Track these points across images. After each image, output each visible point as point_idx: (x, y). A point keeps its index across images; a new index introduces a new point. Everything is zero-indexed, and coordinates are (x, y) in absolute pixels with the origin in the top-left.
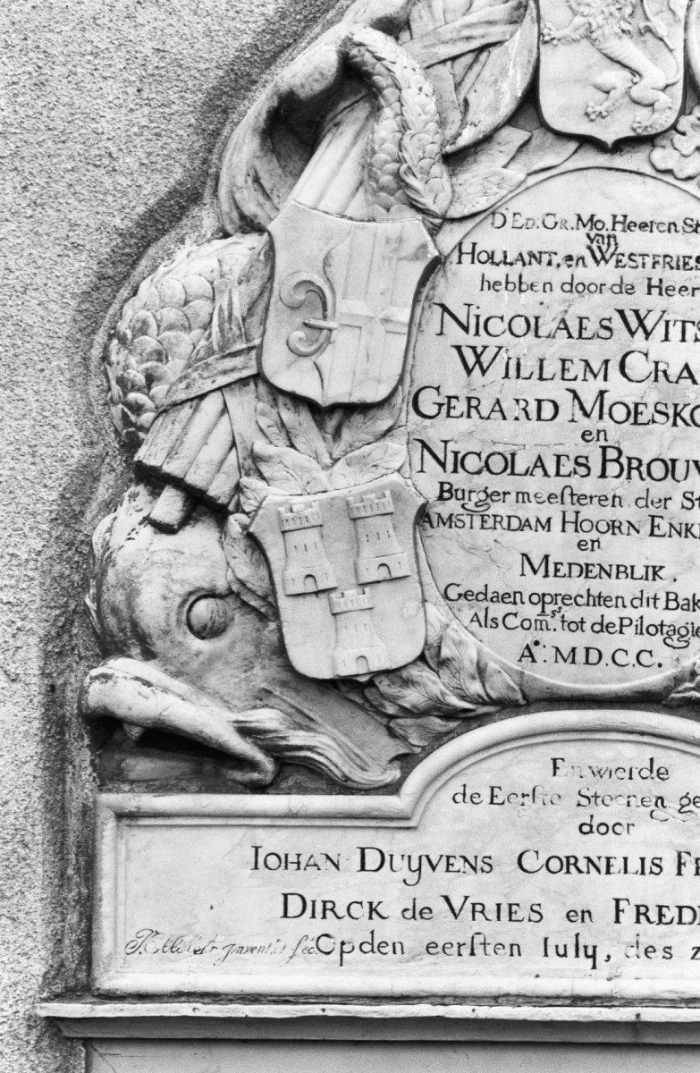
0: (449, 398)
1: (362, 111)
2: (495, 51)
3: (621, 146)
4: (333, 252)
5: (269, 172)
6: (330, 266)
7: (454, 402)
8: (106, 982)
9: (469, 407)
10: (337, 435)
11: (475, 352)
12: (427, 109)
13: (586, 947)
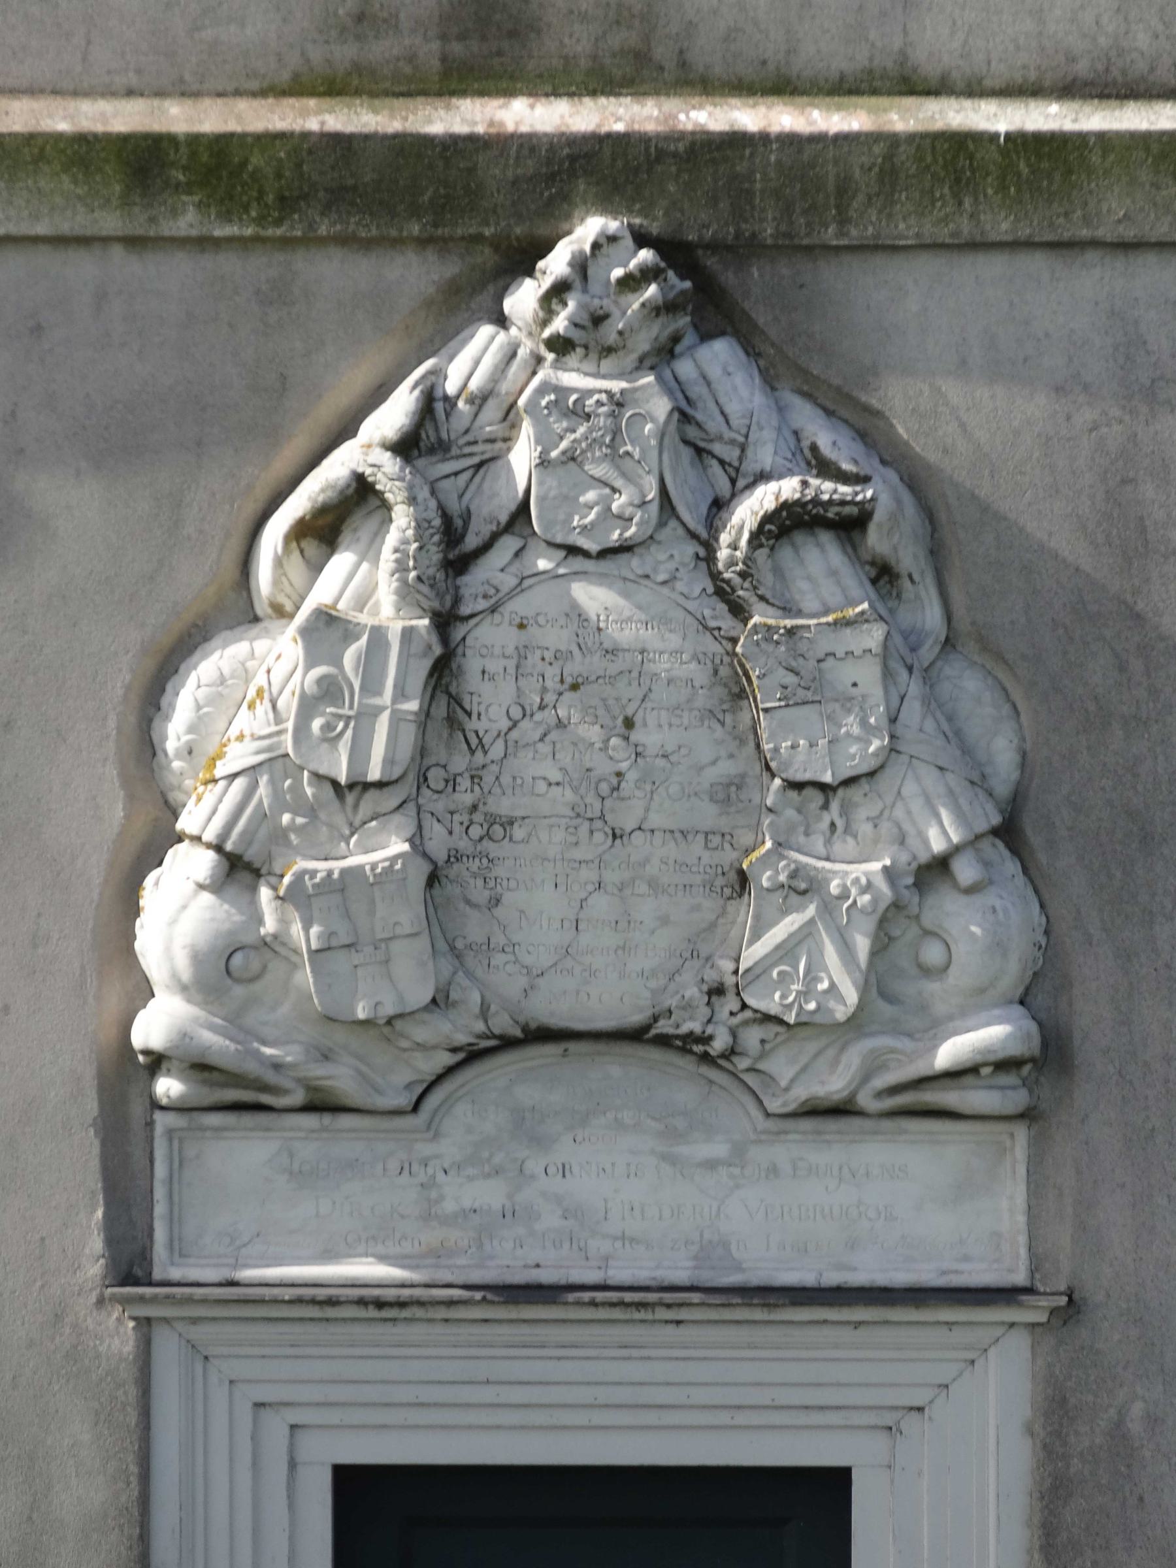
0: (455, 776)
1: (372, 524)
2: (492, 465)
3: (605, 553)
4: (472, 508)
5: (296, 567)
6: (842, 78)
7: (459, 779)
8: (157, 1275)
9: (473, 783)
10: (356, 806)
11: (478, 736)
12: (433, 524)
13: (579, 1240)
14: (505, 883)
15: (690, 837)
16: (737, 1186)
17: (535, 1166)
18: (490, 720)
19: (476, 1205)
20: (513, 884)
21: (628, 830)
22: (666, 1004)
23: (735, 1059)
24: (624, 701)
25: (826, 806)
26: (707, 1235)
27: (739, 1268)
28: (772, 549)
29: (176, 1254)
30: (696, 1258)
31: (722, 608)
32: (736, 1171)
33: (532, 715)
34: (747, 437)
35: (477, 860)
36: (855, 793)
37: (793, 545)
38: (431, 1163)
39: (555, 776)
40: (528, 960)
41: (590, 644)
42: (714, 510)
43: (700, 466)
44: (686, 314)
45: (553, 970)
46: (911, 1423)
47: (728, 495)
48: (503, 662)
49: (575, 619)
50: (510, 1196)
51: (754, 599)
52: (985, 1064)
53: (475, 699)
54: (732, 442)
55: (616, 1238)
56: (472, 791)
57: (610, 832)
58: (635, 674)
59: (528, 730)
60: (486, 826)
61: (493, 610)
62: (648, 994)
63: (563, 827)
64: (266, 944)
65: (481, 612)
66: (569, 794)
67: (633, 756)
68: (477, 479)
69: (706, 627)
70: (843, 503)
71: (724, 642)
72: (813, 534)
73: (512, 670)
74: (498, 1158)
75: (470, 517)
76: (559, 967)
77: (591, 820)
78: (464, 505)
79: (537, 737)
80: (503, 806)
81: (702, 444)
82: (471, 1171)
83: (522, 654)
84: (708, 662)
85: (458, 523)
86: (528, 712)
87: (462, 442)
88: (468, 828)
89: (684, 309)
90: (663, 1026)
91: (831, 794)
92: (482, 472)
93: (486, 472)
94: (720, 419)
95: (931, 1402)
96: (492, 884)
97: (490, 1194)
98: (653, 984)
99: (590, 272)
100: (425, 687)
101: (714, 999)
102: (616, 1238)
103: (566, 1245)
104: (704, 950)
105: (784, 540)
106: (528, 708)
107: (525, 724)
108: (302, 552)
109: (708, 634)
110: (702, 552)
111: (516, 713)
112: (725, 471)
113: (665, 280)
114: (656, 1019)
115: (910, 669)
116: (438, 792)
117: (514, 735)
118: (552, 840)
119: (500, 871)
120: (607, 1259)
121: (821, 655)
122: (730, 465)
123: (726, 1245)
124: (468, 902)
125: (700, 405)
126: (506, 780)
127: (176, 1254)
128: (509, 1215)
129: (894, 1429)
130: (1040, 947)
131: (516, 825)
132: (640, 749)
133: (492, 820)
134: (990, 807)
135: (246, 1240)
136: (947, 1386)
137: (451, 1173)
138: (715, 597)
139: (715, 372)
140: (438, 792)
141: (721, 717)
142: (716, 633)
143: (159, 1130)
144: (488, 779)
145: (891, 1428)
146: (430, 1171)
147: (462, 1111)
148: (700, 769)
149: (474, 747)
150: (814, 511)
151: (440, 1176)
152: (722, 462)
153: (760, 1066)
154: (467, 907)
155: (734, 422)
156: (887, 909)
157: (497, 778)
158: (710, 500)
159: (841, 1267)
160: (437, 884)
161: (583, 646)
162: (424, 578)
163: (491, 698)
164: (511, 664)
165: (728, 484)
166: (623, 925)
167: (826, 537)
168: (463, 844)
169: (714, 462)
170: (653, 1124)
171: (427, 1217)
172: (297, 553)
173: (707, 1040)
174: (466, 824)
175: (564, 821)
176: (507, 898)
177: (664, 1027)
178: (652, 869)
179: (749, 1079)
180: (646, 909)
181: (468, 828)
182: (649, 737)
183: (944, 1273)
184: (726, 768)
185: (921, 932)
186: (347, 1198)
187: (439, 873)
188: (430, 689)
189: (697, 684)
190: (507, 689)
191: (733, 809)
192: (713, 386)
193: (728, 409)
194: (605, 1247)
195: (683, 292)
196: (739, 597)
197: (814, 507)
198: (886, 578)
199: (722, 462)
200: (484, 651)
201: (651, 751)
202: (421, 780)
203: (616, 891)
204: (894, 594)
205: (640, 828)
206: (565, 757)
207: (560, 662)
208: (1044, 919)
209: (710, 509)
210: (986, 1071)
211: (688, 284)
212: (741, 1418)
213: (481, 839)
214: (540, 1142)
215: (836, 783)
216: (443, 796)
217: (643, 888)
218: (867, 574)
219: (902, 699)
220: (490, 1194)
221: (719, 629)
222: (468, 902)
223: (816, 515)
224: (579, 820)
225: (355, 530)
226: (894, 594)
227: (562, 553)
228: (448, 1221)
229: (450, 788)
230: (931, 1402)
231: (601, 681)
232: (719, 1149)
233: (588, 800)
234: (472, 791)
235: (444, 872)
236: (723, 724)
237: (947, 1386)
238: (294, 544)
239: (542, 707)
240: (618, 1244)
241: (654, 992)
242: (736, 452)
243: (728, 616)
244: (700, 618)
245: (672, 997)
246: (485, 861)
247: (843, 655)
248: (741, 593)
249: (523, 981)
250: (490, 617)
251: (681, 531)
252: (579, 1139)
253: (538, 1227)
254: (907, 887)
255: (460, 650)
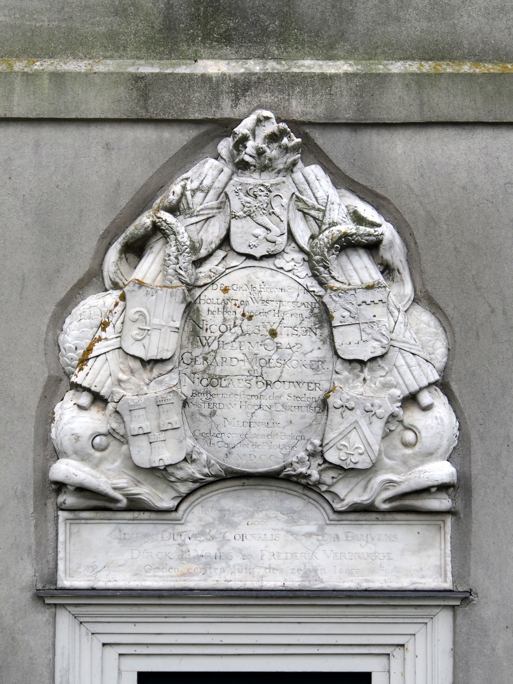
3: (263, 258)
7: (197, 359)
12: (186, 244)
14: (218, 405)
15: (301, 385)
16: (321, 545)
17: (229, 536)
18: (211, 332)
19: (203, 554)
20: (221, 406)
21: (273, 381)
22: (290, 460)
23: (320, 486)
24: (272, 324)
25: (362, 371)
26: (307, 567)
27: (322, 582)
28: (337, 256)
29: (68, 576)
30: (302, 577)
31: (315, 283)
32: (320, 538)
33: (230, 330)
34: (326, 207)
35: (205, 395)
36: (374, 364)
37: (347, 255)
38: (183, 534)
39: (241, 357)
40: (228, 440)
41: (256, 298)
42: (311, 240)
43: (305, 220)
44: (299, 153)
45: (239, 445)
46: (398, 652)
47: (317, 234)
48: (217, 306)
49: (250, 287)
50: (218, 550)
51: (330, 278)
52: (433, 486)
53: (205, 322)
54: (319, 210)
55: (266, 568)
56: (203, 364)
57: (265, 382)
58: (277, 311)
59: (229, 337)
60: (209, 380)
61: (213, 283)
62: (281, 456)
63: (244, 380)
64: (110, 433)
65: (208, 284)
66: (248, 366)
67: (276, 348)
68: (206, 226)
69: (308, 291)
70: (370, 235)
71: (316, 298)
72: (357, 251)
73: (221, 310)
74: (213, 532)
75: (202, 243)
76: (242, 444)
77: (257, 377)
78: (199, 237)
79: (232, 339)
80: (218, 371)
81: (306, 211)
82: (202, 538)
83: (225, 303)
84: (309, 306)
85: (197, 245)
86: (229, 329)
87: (198, 209)
88: (201, 381)
89: (298, 151)
90: (288, 471)
91: (364, 366)
92: (208, 222)
93: (209, 223)
94: (314, 199)
95: (408, 642)
96: (212, 406)
97: (208, 548)
98: (284, 451)
99: (257, 132)
100: (182, 318)
101: (311, 458)
102: (266, 568)
103: (244, 571)
104: (307, 437)
105: (343, 253)
106: (229, 326)
107: (228, 334)
108: (127, 259)
109: (309, 294)
110: (306, 258)
111: (223, 328)
112: (316, 222)
113: (290, 137)
114: (285, 467)
115: (399, 310)
116: (188, 364)
117: (222, 339)
118: (238, 386)
119: (216, 400)
120: (262, 577)
121: (360, 302)
122: (319, 220)
123: (315, 571)
124: (201, 414)
125: (305, 193)
126: (218, 359)
127: (68, 576)
128: (218, 558)
129: (391, 655)
130: (456, 436)
131: (223, 379)
132: (279, 345)
133: (211, 377)
134: (435, 371)
135: (100, 569)
136: (414, 635)
137: (192, 539)
138: (312, 278)
139: (312, 178)
140: (188, 364)
141: (314, 331)
142: (312, 293)
143: (61, 519)
144: (210, 358)
145: (389, 654)
146: (183, 538)
147: (197, 511)
148: (305, 354)
149: (204, 344)
150: (357, 239)
151: (187, 540)
152: (314, 218)
153: (332, 489)
154: (201, 417)
155: (320, 201)
156: (389, 417)
157: (215, 358)
158: (309, 236)
159: (367, 581)
160: (187, 406)
161: (253, 299)
162: (182, 267)
163: (212, 321)
164: (221, 307)
165: (317, 229)
166: (271, 424)
167: (362, 252)
168: (200, 388)
169: (311, 219)
170: (283, 516)
171: (181, 558)
172: (124, 259)
173: (307, 476)
174: (200, 379)
175: (244, 377)
176: (219, 412)
177: (289, 471)
178: (284, 399)
179: (327, 496)
180: (282, 417)
181: (201, 381)
182: (283, 339)
183: (414, 583)
184: (317, 354)
185: (403, 428)
186: (145, 550)
187: (188, 401)
188: (184, 318)
189: (304, 316)
190: (219, 318)
191: (320, 373)
192: (311, 185)
193: (318, 195)
194: (262, 571)
195: (298, 143)
196: (323, 277)
197: (357, 236)
198: (387, 271)
199: (314, 218)
200: (209, 301)
201: (284, 346)
202: (181, 359)
203: (268, 409)
204: (391, 278)
205: (278, 381)
206: (246, 349)
207: (243, 306)
208: (458, 424)
209: (309, 240)
210: (433, 490)
211: (299, 140)
212: (322, 650)
213: (207, 386)
214: (233, 525)
215: (366, 360)
216: (190, 366)
217: (280, 408)
218: (379, 268)
219: (396, 323)
220: (208, 548)
221: (314, 291)
222: (201, 414)
223: (358, 240)
224: (251, 377)
225: (151, 248)
226: (391, 278)
227: (244, 258)
228: (190, 560)
229: (193, 363)
230: (408, 642)
231: (261, 314)
232: (312, 528)
233: (255, 368)
234: (203, 364)
235: (191, 401)
236: (316, 334)
237: (414, 635)
238: (123, 255)
239: (235, 326)
240: (268, 570)
241: (284, 455)
242: (321, 214)
243: (318, 286)
244: (305, 287)
245: (292, 457)
246: (209, 395)
247: (370, 303)
248: (324, 275)
249: (225, 450)
250: (212, 286)
251: (297, 248)
252: (249, 523)
253: (232, 563)
254: (398, 407)
255: (198, 301)
